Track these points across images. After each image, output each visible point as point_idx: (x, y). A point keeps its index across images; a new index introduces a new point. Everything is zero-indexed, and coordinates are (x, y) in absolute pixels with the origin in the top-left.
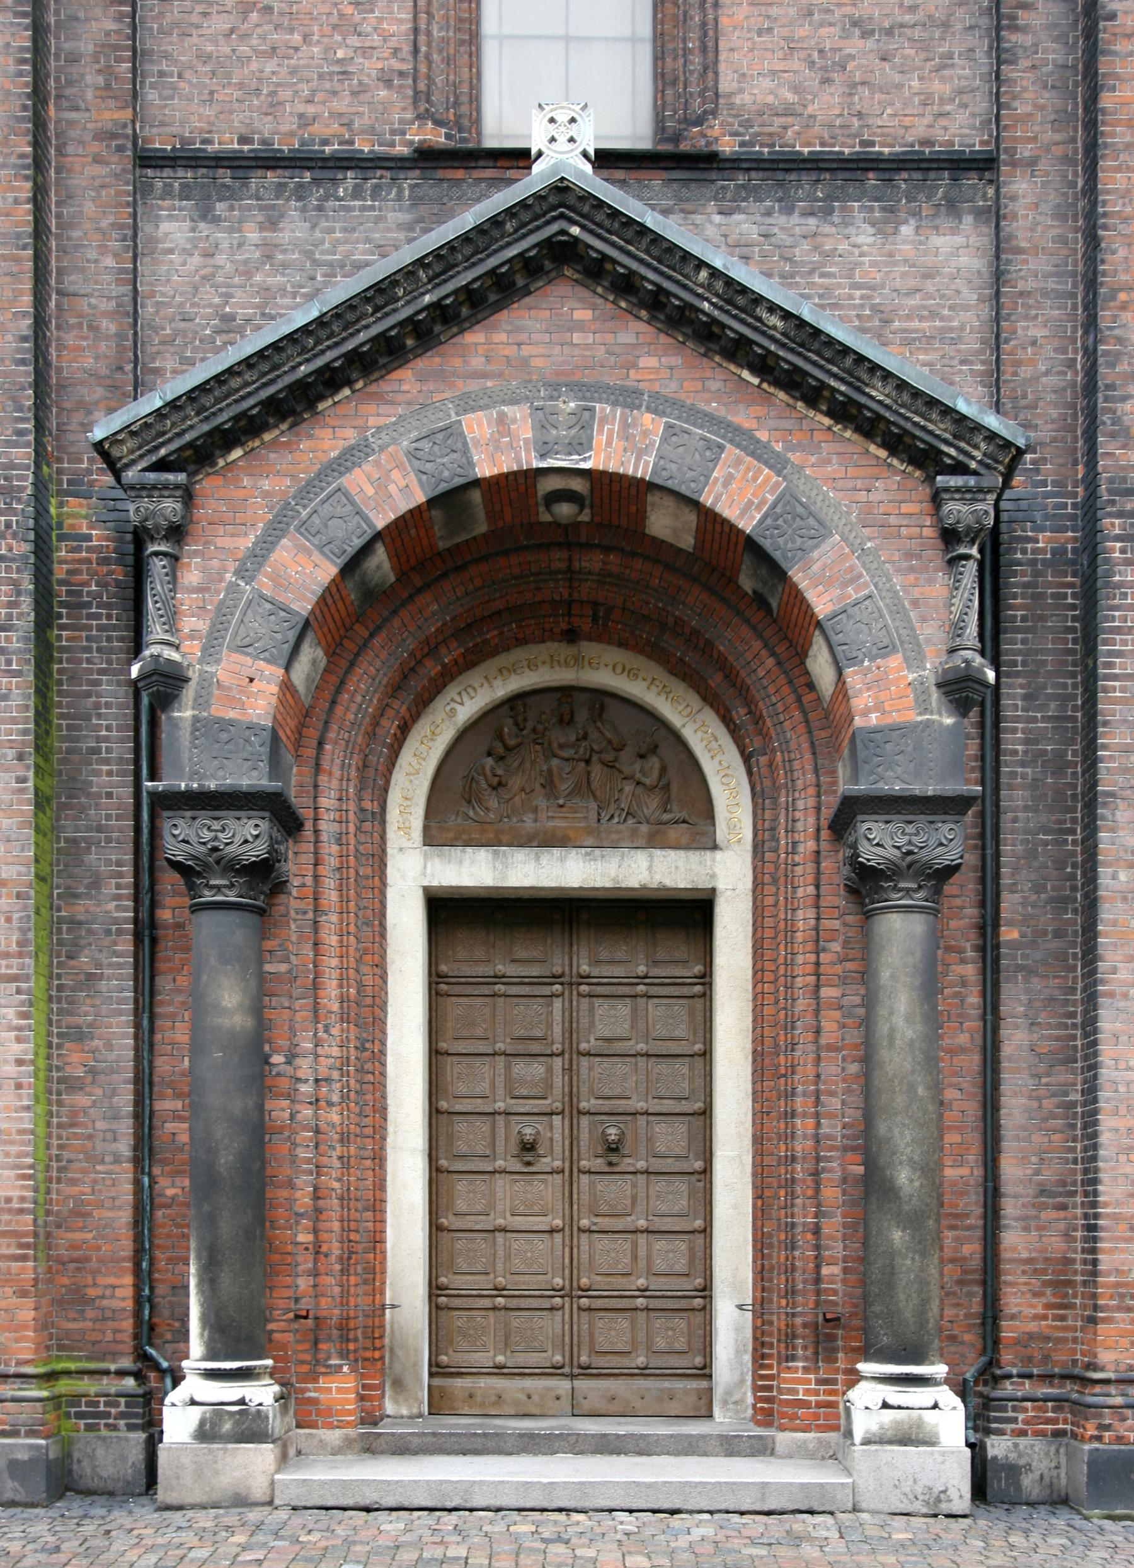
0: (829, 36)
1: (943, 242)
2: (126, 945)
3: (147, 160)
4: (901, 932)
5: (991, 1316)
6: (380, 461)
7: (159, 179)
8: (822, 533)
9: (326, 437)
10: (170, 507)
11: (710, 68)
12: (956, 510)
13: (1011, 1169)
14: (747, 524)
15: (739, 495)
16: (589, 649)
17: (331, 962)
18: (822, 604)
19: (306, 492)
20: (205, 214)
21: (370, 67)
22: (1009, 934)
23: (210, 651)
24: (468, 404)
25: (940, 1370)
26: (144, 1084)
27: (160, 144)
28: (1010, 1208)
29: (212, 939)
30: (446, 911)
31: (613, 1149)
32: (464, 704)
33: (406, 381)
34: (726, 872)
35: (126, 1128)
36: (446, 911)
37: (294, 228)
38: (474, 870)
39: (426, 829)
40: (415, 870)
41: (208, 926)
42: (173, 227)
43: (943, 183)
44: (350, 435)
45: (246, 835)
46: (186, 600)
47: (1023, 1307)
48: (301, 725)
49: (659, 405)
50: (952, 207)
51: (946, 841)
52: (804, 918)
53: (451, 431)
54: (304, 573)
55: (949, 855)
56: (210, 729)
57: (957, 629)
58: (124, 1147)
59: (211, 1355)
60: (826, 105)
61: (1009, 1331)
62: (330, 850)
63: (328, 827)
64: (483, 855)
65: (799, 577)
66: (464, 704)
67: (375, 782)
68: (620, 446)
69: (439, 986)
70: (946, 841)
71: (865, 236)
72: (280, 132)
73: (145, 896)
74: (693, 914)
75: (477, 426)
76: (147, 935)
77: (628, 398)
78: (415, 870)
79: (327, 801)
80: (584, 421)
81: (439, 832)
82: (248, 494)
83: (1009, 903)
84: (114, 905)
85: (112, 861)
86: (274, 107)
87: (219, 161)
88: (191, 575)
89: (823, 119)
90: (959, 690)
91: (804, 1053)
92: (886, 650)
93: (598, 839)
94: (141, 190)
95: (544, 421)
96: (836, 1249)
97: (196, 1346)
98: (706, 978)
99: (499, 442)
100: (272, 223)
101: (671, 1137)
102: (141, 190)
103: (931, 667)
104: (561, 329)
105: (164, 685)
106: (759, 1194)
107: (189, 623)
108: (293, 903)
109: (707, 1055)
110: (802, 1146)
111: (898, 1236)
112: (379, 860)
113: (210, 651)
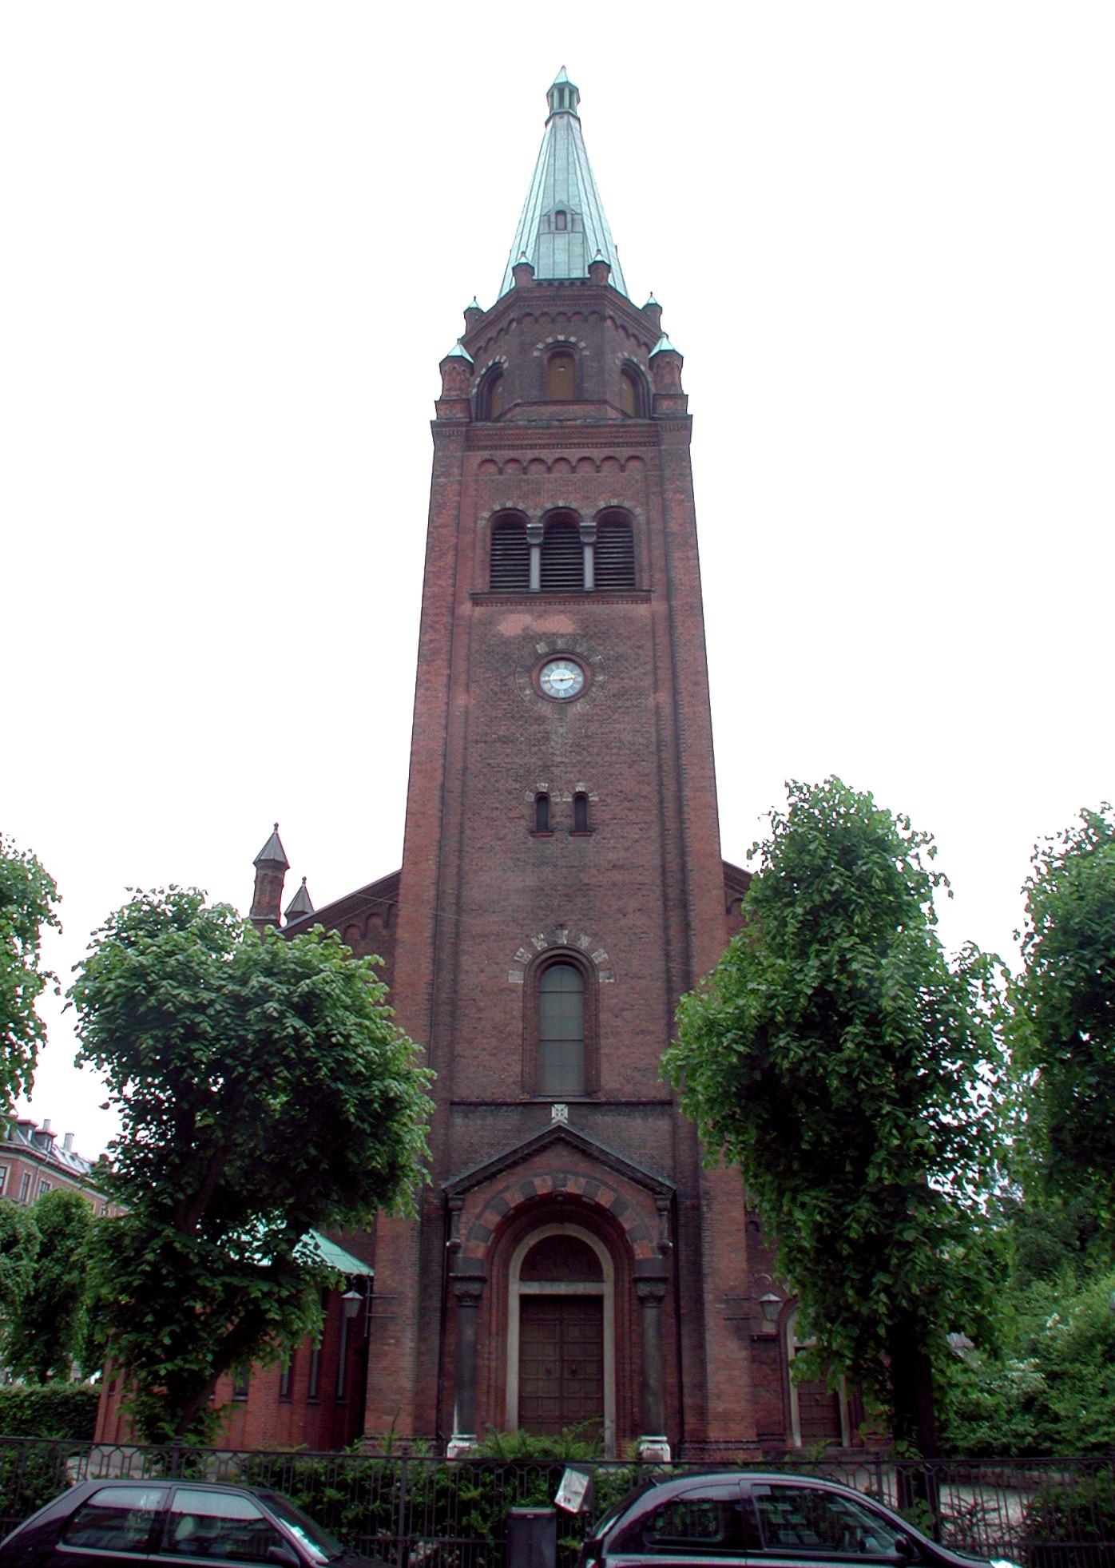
0: (629, 1072)
1: (660, 1122)
2: (438, 1314)
3: (453, 1103)
4: (651, 1314)
5: (681, 1424)
6: (513, 1192)
7: (455, 1108)
8: (626, 1208)
9: (499, 1185)
10: (459, 1203)
11: (598, 1079)
12: (660, 1203)
13: (685, 1379)
14: (607, 1206)
15: (605, 1198)
16: (568, 1225)
17: (494, 1319)
18: (626, 1226)
19: (494, 1198)
20: (466, 1117)
21: (510, 1080)
22: (683, 1311)
23: (468, 1240)
24: (536, 1176)
25: (664, 1438)
26: (442, 1353)
27: (456, 1100)
28: (686, 1391)
29: (466, 1314)
30: (525, 1300)
31: (574, 1372)
32: (531, 1240)
33: (519, 1169)
34: (607, 1289)
35: (436, 1367)
36: (525, 1300)
37: (490, 1120)
38: (533, 1289)
39: (522, 1270)
40: (516, 1288)
41: (463, 1311)
42: (458, 1121)
43: (659, 1108)
44: (504, 1184)
45: (474, 1288)
46: (461, 1225)
47: (691, 1421)
48: (490, 1253)
49: (584, 1176)
50: (662, 1114)
51: (660, 1289)
52: (627, 1306)
53: (532, 1183)
54: (493, 1219)
55: (662, 1293)
56: (466, 1259)
57: (661, 1233)
58: (435, 1372)
59: (461, 1433)
60: (628, 1088)
61: (687, 1427)
62: (495, 1287)
63: (494, 1281)
64: (536, 1284)
65: (621, 1219)
66: (531, 1240)
67: (506, 1266)
68: (573, 1187)
69: (523, 1321)
70: (660, 1289)
71: (639, 1121)
72: (487, 1096)
73: (444, 1301)
74: (597, 1301)
75: (537, 1181)
76: (444, 1312)
77: (576, 1174)
78: (516, 1288)
79: (494, 1273)
80: (565, 1179)
81: (527, 1275)
82: (480, 1197)
83: (683, 1303)
84: (436, 1303)
85: (436, 1291)
86: (485, 1090)
87: (471, 1104)
88: (463, 1220)
89: (628, 1092)
90: (663, 1249)
91: (627, 1343)
92: (644, 1238)
93: (569, 1279)
94: (451, 1111)
95: (554, 1179)
96: (636, 1403)
97: (456, 1430)
98: (602, 1320)
99: (543, 1185)
100: (484, 1119)
101: (591, 1369)
102: (451, 1111)
103: (655, 1243)
104: (558, 1158)
105: (455, 1248)
106: (617, 1385)
107: (463, 1231)
108: (485, 1302)
109: (602, 1343)
110: (627, 1373)
111: (651, 1399)
112: (506, 1287)
113: (468, 1240)
